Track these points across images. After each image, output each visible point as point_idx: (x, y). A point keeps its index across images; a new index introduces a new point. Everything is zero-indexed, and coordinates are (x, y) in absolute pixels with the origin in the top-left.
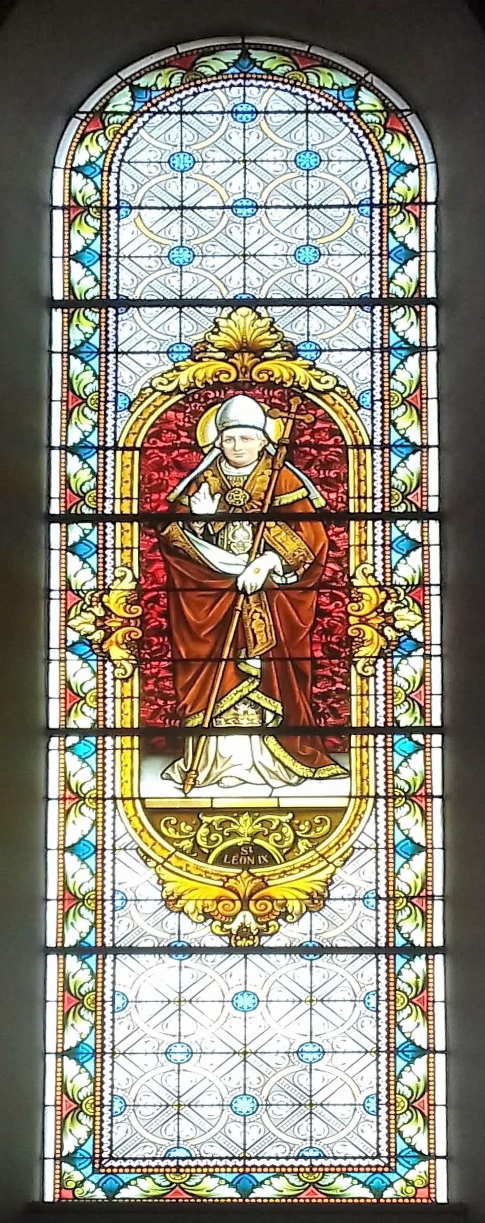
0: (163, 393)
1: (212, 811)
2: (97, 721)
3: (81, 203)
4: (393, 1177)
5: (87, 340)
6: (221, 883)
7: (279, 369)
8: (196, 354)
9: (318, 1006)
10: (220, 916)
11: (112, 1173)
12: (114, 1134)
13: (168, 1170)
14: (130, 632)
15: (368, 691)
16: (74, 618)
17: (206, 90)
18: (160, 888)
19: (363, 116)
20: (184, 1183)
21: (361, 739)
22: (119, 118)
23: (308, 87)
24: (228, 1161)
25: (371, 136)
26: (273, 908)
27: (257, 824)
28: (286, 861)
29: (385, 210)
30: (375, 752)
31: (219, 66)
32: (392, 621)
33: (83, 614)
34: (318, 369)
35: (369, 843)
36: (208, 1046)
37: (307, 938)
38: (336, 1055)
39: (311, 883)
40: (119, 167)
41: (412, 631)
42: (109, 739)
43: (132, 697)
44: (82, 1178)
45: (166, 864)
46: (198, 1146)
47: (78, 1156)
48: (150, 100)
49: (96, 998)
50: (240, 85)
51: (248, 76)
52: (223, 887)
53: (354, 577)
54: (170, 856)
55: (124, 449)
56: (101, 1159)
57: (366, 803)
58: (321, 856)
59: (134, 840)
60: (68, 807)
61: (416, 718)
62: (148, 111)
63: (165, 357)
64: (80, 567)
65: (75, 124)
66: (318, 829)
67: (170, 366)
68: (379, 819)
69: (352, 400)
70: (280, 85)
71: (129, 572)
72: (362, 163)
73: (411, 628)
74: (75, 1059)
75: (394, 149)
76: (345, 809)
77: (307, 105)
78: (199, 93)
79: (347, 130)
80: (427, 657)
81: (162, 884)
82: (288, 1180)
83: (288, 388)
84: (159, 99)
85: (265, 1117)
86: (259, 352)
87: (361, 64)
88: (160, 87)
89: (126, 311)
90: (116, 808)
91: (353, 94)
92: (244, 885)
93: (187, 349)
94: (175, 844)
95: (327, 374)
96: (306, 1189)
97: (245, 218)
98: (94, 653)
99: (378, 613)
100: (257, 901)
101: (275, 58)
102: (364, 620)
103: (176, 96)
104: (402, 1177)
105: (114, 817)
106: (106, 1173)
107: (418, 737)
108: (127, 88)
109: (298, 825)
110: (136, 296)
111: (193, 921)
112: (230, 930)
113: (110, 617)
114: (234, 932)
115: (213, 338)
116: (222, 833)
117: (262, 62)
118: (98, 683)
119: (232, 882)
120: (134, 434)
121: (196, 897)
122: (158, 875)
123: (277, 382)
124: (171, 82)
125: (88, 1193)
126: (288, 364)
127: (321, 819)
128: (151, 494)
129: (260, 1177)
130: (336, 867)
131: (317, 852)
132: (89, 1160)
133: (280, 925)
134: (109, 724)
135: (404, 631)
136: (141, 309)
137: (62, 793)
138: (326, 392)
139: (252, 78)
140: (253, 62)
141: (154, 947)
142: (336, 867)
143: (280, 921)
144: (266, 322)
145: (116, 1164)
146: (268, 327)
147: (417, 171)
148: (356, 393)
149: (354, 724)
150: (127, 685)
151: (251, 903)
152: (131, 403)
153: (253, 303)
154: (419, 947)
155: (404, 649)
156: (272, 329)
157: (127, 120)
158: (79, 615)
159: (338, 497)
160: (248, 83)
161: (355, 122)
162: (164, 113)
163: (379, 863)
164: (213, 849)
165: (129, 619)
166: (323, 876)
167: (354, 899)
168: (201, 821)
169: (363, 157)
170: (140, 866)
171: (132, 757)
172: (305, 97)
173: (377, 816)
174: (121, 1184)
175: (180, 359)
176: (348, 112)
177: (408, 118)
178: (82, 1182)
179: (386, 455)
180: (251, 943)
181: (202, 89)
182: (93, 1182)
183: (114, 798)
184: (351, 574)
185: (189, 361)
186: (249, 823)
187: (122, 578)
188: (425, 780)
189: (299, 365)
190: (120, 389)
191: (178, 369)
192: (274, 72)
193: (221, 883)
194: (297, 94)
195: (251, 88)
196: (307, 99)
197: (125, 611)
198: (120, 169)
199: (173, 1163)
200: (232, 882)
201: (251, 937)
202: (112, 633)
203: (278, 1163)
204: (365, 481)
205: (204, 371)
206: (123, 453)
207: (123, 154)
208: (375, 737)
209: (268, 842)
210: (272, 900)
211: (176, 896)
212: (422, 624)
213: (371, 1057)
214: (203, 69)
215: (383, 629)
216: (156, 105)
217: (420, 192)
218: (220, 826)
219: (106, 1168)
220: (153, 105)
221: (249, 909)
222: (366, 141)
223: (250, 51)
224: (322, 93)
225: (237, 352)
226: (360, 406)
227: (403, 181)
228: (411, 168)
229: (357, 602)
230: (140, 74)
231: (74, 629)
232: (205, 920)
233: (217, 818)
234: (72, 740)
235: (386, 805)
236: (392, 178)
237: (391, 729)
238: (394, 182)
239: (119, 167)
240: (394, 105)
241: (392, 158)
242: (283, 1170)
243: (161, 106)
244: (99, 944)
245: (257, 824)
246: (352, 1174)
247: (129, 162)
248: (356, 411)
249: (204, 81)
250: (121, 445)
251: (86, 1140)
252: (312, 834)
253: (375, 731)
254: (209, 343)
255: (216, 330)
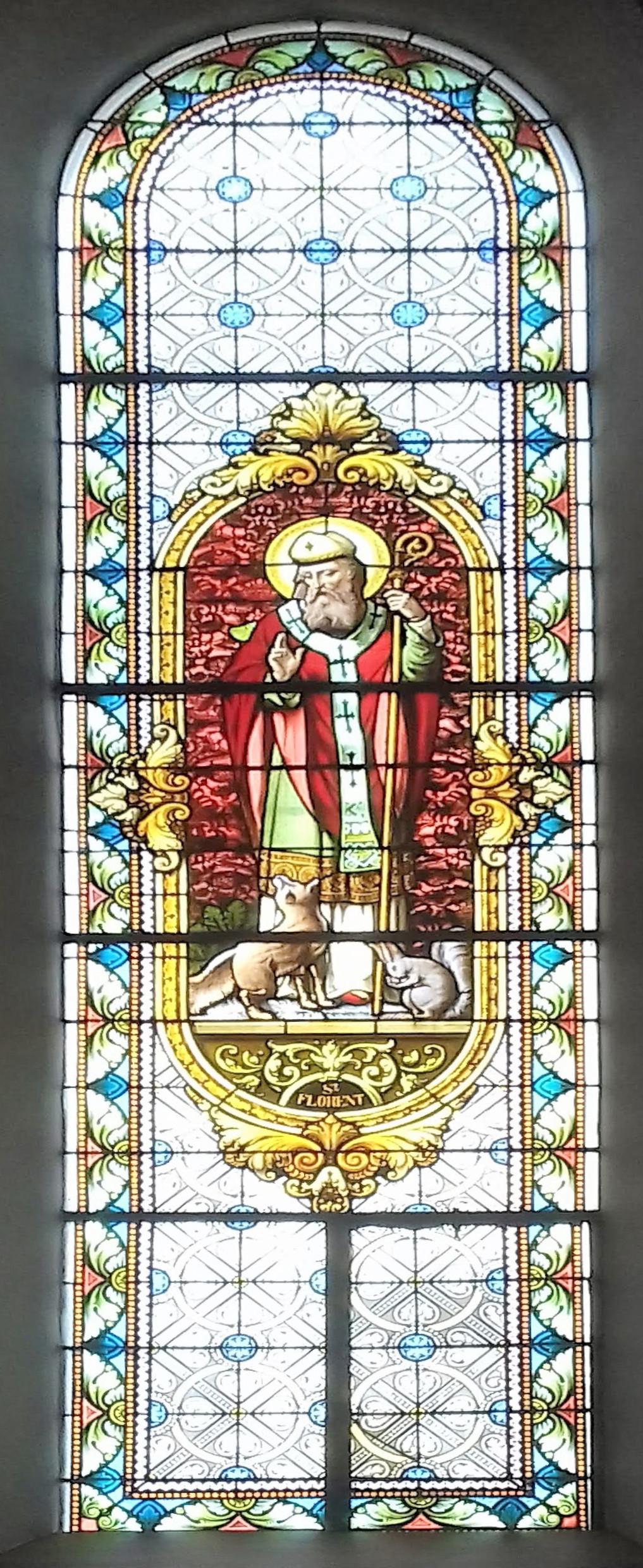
0: (216, 497)
1: (286, 1037)
2: (130, 925)
3: (98, 242)
4: (530, 1502)
5: (110, 427)
6: (299, 1131)
7: (373, 464)
8: (260, 445)
9: (231, 1275)
10: (296, 1172)
11: (149, 1499)
12: (151, 1450)
13: (223, 1495)
14: (174, 810)
15: (497, 886)
16: (98, 791)
17: (268, 95)
18: (216, 1137)
19: (485, 127)
20: (248, 1511)
21: (488, 947)
22: (147, 130)
23: (410, 90)
24: (302, 1482)
25: (496, 156)
26: (370, 1163)
27: (347, 1054)
28: (385, 1104)
29: (515, 255)
30: (508, 963)
31: (285, 61)
32: (528, 795)
33: (109, 786)
34: (427, 467)
35: (497, 1078)
36: (278, 1340)
37: (416, 1200)
38: (206, 1344)
39: (422, 1134)
40: (150, 196)
41: (557, 806)
42: (147, 948)
43: (178, 894)
44: (110, 1504)
45: (224, 1106)
46: (264, 1465)
47: (103, 1475)
48: (190, 107)
49: (127, 1277)
50: (315, 88)
51: (326, 75)
52: (301, 1135)
53: (477, 738)
54: (230, 1095)
55: (164, 569)
56: (134, 1480)
57: (495, 1029)
58: (433, 1095)
59: (180, 1076)
60: (90, 1032)
61: (562, 921)
62: (188, 120)
63: (217, 450)
64: (105, 722)
65: (86, 137)
66: (430, 1061)
67: (224, 460)
68: (512, 1049)
69: (474, 506)
70: (370, 87)
71: (172, 732)
72: (483, 191)
73: (555, 803)
74: (99, 1354)
75: (526, 172)
76: (468, 1034)
77: (408, 114)
78: (258, 97)
79: (464, 148)
80: (577, 846)
81: (218, 1132)
82: (388, 1505)
83: (387, 491)
84: (202, 105)
85: (176, 1429)
86: (347, 443)
87: (481, 57)
88: (203, 89)
89: (163, 387)
90: (155, 1032)
91: (470, 98)
92: (331, 1136)
93: (247, 438)
94: (235, 1080)
95: (439, 473)
96: (232, 1519)
97: (323, 265)
98: (125, 837)
99: (511, 786)
100: (347, 1152)
101: (362, 51)
102: (490, 793)
103: (227, 102)
104: (543, 1503)
105: (153, 1046)
106: (140, 1498)
107: (567, 945)
108: (157, 91)
109: (403, 1055)
110: (348, 368)
111: (261, 1179)
112: (311, 1190)
113: (147, 790)
114: (316, 1194)
115: (283, 425)
116: (298, 1065)
117: (346, 58)
118: (131, 876)
119: (313, 1129)
120: (177, 550)
121: (264, 1149)
122: (213, 1120)
123: (371, 483)
124: (217, 84)
125: (116, 1523)
126: (388, 459)
127: (433, 1049)
128: (200, 633)
129: (169, 1505)
130: (453, 1110)
131: (428, 1091)
132: (118, 1482)
133: (377, 1184)
134: (147, 928)
135: (545, 807)
136: (184, 386)
137: (83, 1013)
138: (438, 496)
139: (330, 78)
140: (333, 58)
141: (208, 1213)
142: (453, 1110)
143: (379, 1179)
144: (358, 402)
145: (153, 1487)
146: (358, 410)
147: (555, 200)
148: (480, 498)
149: (478, 928)
150: (172, 879)
151: (340, 1156)
152: (171, 511)
153: (337, 378)
154: (566, 1211)
155: (546, 831)
156: (365, 414)
157: (159, 132)
158: (104, 787)
159: (456, 637)
160: (326, 84)
161: (475, 136)
162: (210, 124)
163: (500, 333)
164: (286, 1087)
165: (172, 793)
166: (437, 1120)
167: (478, 1150)
168: (271, 1049)
169: (485, 184)
170: (189, 1110)
171: (178, 969)
172: (404, 102)
173: (509, 1045)
174: (162, 1513)
175: (238, 452)
176: (465, 123)
177: (548, 131)
178: (110, 1509)
179: (520, 450)
180: (338, 1207)
181: (262, 92)
182: (124, 1510)
183: (153, 1021)
184: (474, 733)
185: (251, 455)
186: (335, 1053)
187: (163, 740)
188: (575, 1127)
189: (402, 461)
190: (156, 491)
191: (235, 466)
192: (362, 71)
193: (299, 1131)
194: (393, 99)
195: (331, 91)
196: (408, 107)
197: (167, 783)
198: (150, 200)
199: (230, 1486)
200: (313, 1129)
201: (339, 1200)
202: (150, 812)
203: (191, 1487)
204: (496, 1000)
205: (273, 467)
206: (161, 576)
207: (154, 179)
208: (508, 943)
209: (360, 1076)
210: (368, 1152)
211: (236, 1148)
212: (569, 799)
213: (159, 1341)
214: (260, 66)
215: (517, 805)
216: (199, 113)
217: (560, 226)
218: (296, 1055)
219: (141, 1493)
220: (195, 114)
221: (336, 1164)
222: (488, 163)
223: (327, 43)
224: (428, 99)
225: (318, 443)
226: (485, 516)
227: (537, 214)
228: (549, 196)
229: (482, 770)
230: (174, 73)
231: (98, 807)
232: (278, 1177)
233: (291, 1049)
234: (92, 948)
235: (522, 1031)
236: (524, 209)
237: (529, 934)
238: (526, 216)
239: (150, 196)
240: (528, 114)
241: (524, 183)
242: (382, 1494)
243: (205, 115)
244: (135, 1209)
245: (347, 1054)
246: (478, 1499)
247: (162, 189)
248: (479, 521)
249: (265, 82)
250: (159, 565)
251: (115, 1456)
252: (421, 1069)
253: (506, 936)
254: (278, 430)
255: (287, 413)
